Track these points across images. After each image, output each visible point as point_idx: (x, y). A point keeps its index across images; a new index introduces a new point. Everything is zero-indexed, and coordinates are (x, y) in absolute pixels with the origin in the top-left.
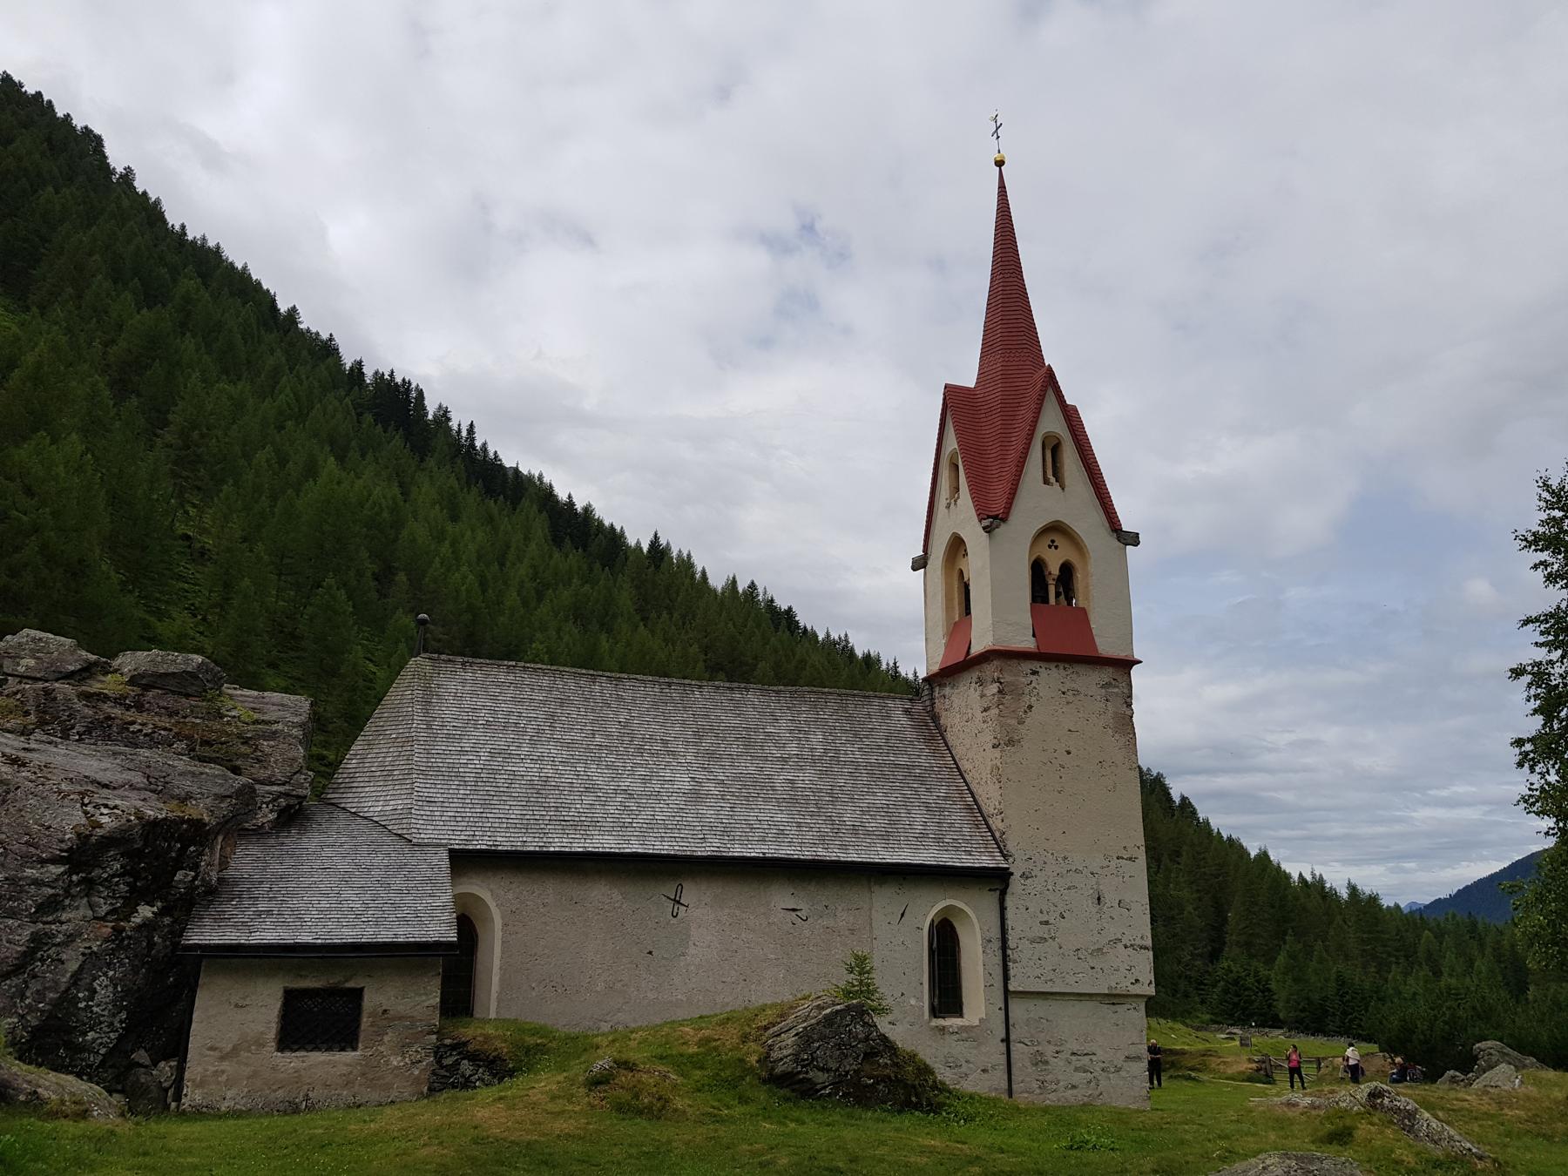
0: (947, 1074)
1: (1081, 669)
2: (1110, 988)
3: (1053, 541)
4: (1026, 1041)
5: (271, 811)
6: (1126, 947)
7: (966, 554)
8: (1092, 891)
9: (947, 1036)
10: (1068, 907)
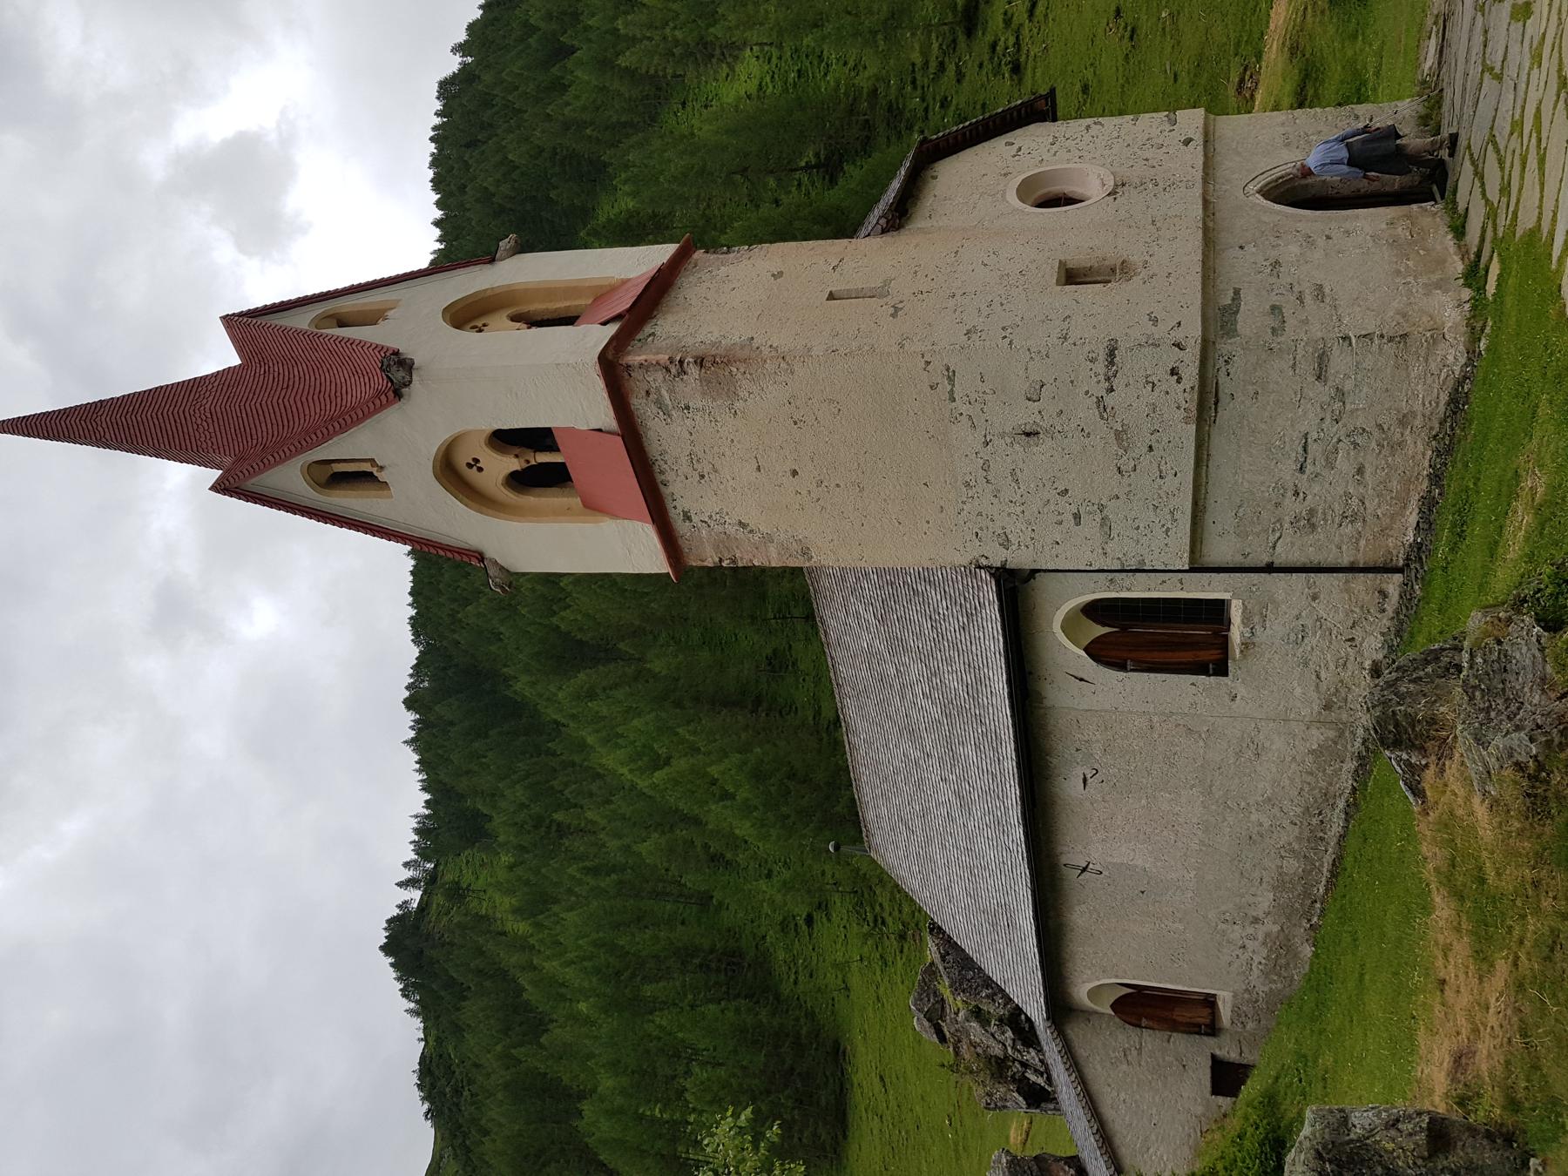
0: (1314, 642)
1: (653, 449)
2: (1186, 421)
3: (469, 466)
4: (1272, 539)
5: (1028, 1052)
6: (1112, 390)
7: (529, 328)
8: (1017, 447)
9: (1256, 640)
10: (1048, 484)
